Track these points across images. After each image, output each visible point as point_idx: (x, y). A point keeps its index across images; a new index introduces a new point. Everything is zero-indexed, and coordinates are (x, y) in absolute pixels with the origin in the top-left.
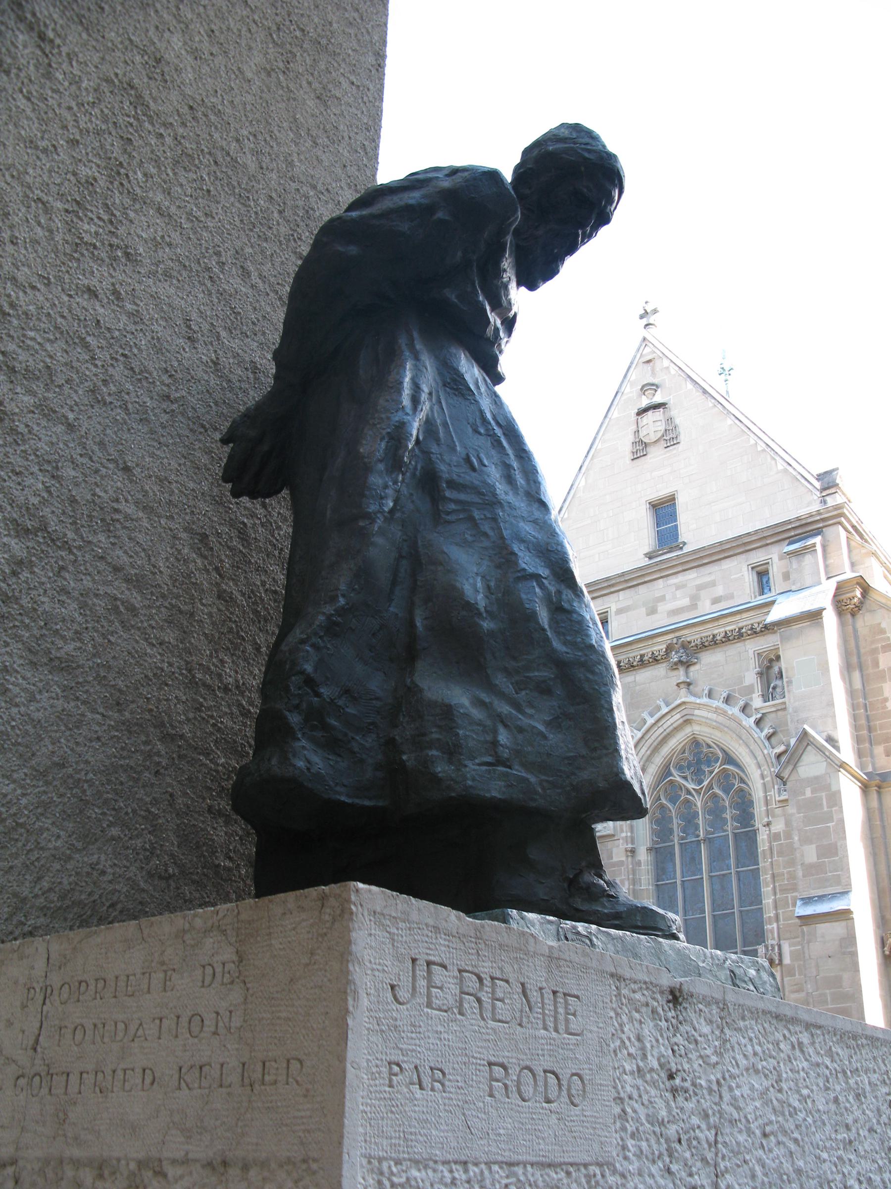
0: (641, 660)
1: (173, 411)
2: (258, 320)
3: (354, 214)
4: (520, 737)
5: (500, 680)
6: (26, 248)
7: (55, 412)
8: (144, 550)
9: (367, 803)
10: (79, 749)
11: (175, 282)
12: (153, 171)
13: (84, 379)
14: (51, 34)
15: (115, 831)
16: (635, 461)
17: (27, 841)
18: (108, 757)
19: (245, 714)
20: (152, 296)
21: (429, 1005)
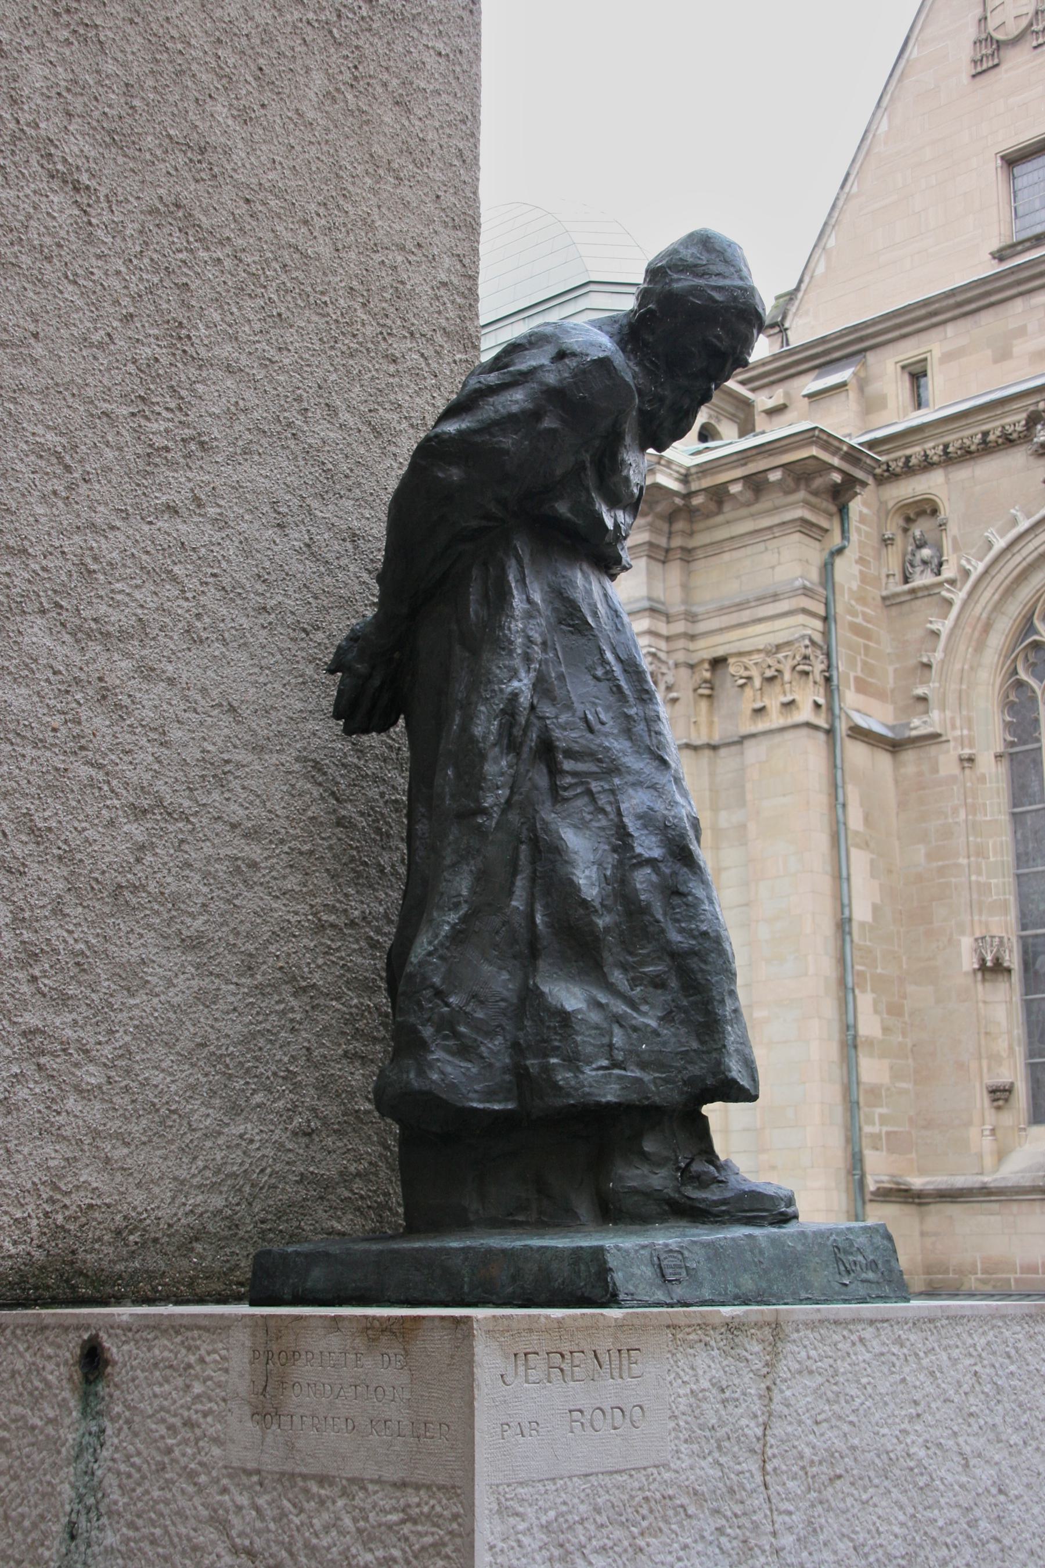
0: (984, 442)
1: (270, 623)
2: (352, 470)
3: (451, 427)
4: (635, 1035)
5: (617, 977)
6: (99, 481)
7: (153, 670)
8: (258, 796)
9: (496, 1107)
10: (217, 1025)
11: (256, 457)
12: (217, 317)
13: (177, 619)
14: (85, 178)
15: (258, 1098)
16: (978, 79)
17: (181, 1125)
18: (246, 1026)
19: (374, 945)
20: (233, 487)
21: (527, 1382)
